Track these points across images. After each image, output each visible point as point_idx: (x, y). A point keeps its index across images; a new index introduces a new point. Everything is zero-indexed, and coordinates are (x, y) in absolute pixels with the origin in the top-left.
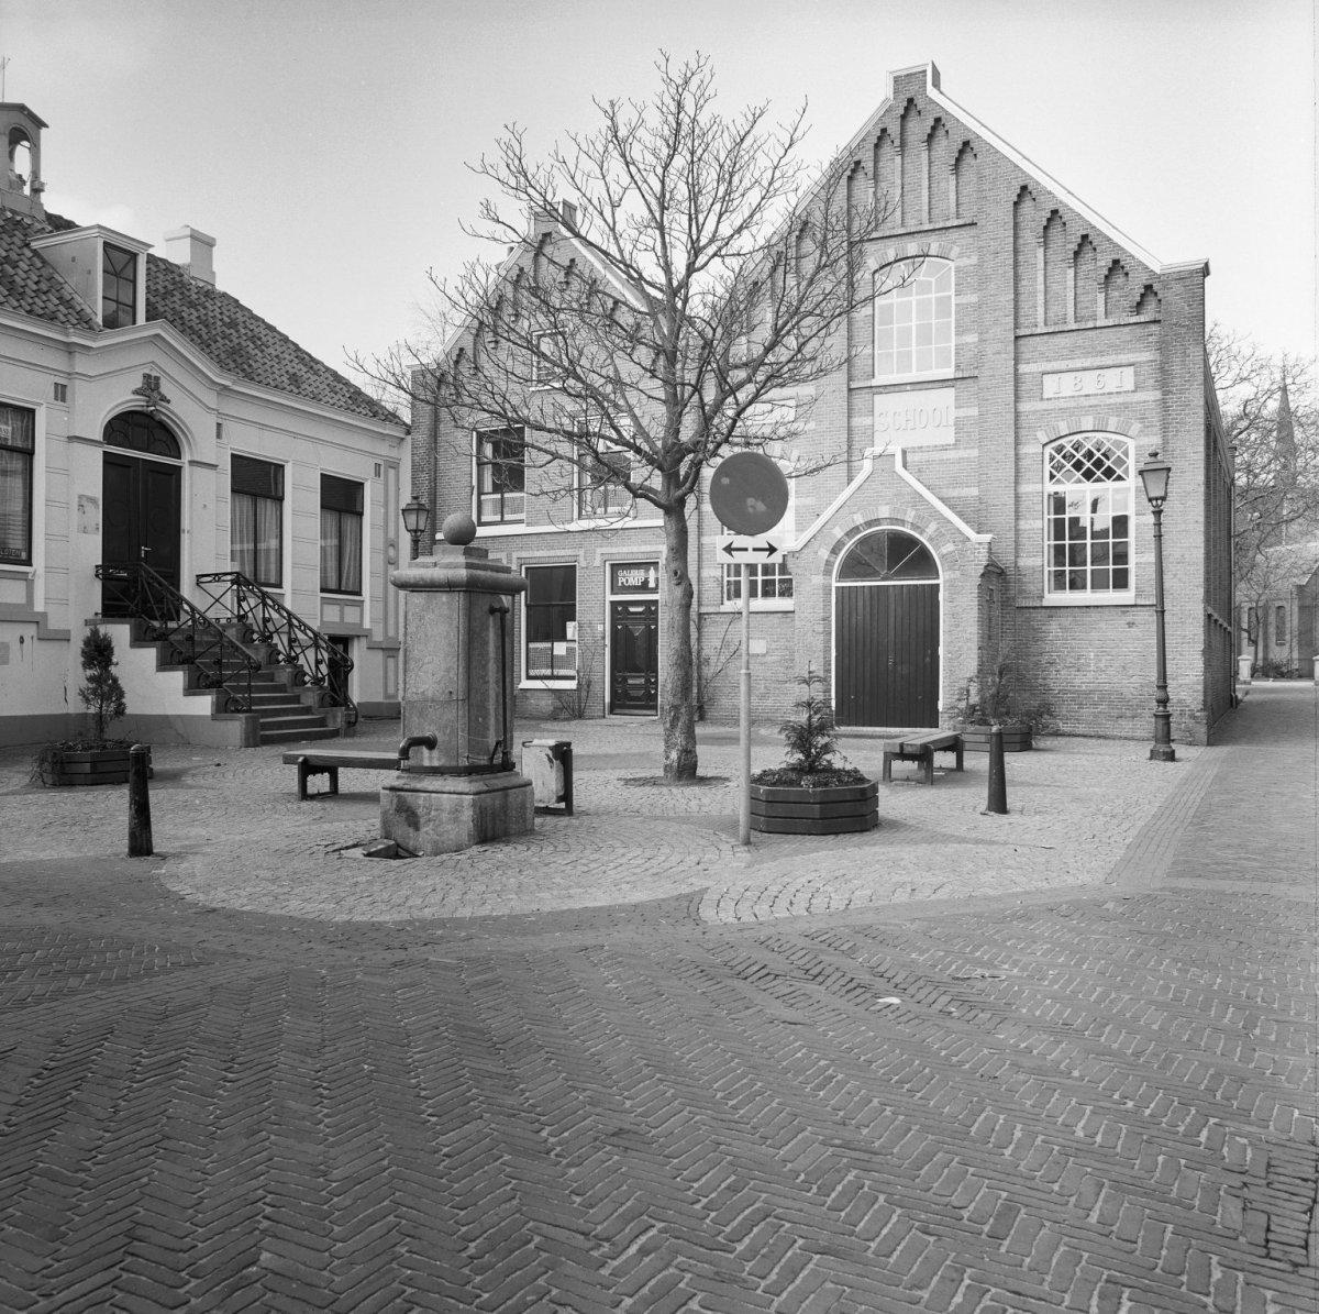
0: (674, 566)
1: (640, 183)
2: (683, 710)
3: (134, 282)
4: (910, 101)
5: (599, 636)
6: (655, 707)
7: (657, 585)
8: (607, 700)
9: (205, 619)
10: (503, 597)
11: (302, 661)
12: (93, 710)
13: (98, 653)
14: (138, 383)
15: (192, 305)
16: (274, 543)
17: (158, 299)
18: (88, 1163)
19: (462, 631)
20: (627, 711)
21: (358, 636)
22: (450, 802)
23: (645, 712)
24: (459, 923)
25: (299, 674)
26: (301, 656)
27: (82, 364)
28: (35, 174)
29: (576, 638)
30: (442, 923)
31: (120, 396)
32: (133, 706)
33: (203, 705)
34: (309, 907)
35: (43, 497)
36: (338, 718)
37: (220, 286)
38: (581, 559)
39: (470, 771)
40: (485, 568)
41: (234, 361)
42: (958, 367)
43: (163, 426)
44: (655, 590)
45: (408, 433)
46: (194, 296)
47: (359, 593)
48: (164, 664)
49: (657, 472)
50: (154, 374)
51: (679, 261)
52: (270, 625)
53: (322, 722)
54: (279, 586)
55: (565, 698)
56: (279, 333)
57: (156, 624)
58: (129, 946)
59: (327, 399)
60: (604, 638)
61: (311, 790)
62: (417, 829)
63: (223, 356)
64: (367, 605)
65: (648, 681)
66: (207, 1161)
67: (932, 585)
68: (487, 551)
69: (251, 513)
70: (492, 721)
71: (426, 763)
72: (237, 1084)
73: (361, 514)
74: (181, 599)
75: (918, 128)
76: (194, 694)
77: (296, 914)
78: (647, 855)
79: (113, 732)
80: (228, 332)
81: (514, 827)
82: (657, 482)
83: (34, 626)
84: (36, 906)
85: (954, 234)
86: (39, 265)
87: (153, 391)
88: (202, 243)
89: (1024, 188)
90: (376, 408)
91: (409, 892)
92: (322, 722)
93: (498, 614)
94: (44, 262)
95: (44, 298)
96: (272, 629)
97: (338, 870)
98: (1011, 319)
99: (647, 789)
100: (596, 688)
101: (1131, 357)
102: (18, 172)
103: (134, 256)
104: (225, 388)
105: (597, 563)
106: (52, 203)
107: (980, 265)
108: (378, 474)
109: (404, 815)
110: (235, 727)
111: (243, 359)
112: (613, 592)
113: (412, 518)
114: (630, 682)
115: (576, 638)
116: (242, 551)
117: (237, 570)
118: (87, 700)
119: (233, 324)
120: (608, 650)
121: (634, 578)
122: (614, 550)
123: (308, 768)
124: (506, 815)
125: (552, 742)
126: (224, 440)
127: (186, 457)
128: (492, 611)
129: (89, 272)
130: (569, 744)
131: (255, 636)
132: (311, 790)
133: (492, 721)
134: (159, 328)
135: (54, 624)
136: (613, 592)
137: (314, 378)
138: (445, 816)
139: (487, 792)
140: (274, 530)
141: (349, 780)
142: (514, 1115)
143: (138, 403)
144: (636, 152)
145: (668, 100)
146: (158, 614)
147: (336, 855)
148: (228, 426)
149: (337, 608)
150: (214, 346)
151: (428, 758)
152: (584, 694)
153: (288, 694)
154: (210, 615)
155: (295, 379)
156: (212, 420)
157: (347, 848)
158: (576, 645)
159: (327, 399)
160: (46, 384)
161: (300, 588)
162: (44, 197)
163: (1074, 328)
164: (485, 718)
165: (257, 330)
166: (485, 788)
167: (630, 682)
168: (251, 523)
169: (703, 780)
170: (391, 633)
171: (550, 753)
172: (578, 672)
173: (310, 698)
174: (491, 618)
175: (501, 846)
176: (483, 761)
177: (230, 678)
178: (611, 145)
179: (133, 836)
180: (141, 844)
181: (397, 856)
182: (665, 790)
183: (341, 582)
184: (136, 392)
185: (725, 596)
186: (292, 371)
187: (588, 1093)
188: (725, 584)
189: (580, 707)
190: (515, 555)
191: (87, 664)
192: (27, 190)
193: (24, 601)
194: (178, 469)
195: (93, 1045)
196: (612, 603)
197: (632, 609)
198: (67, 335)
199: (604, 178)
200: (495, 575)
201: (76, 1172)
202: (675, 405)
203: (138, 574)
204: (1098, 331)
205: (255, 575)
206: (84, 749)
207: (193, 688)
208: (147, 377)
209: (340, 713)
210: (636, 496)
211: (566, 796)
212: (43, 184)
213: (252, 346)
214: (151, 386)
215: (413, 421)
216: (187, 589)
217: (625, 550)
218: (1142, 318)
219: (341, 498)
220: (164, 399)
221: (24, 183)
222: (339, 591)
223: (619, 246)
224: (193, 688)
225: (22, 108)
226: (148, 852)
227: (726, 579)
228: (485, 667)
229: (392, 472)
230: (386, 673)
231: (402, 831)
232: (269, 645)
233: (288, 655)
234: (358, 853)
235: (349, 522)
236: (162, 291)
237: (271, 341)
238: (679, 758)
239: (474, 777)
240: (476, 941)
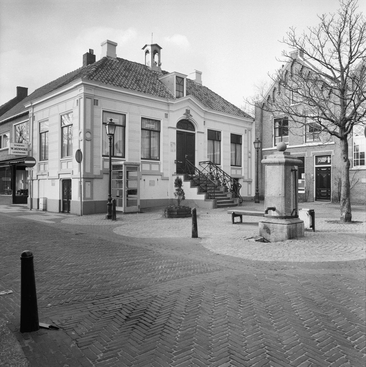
0: (344, 156)
1: (332, 39)
2: (347, 200)
3: (183, 86)
5: (312, 178)
6: (330, 199)
7: (330, 162)
8: (314, 196)
9: (202, 173)
10: (295, 166)
11: (227, 185)
12: (177, 198)
13: (178, 183)
14: (185, 112)
15: (197, 90)
16: (218, 153)
17: (188, 89)
18: (210, 327)
19: (283, 177)
20: (320, 200)
21: (241, 178)
22: (281, 228)
23: (326, 200)
24: (291, 264)
25: (226, 188)
26: (227, 184)
27: (171, 108)
28: (159, 61)
29: (305, 178)
30: (285, 263)
31: (180, 116)
32: (187, 197)
33: (202, 197)
34: (244, 255)
35: (128, 149)
36: (237, 201)
37: (203, 85)
38: (306, 155)
39: (286, 218)
40: (290, 158)
41: (208, 104)
44: (330, 163)
45: (254, 121)
46: (197, 88)
47: (241, 166)
48: (193, 186)
49: (338, 127)
50: (188, 109)
51: (345, 61)
52: (218, 175)
53: (233, 202)
54: (220, 164)
55: (301, 196)
56: (219, 96)
57: (190, 175)
58: (199, 263)
59: (231, 113)
60: (313, 178)
61: (235, 221)
62: (270, 234)
63: (205, 103)
64: (243, 170)
65: (327, 191)
66: (243, 331)
68: (290, 153)
69: (212, 145)
70: (292, 203)
71: (272, 215)
72: (244, 308)
73: (241, 144)
74: (195, 168)
76: (200, 194)
77: (241, 257)
78: (344, 245)
79: (182, 204)
80: (206, 97)
81: (298, 235)
82: (338, 130)
83: (160, 176)
84: (172, 250)
86: (161, 84)
88: (199, 74)
90: (245, 114)
91: (272, 253)
92: (233, 202)
93: (294, 171)
94: (162, 83)
95: (162, 92)
96: (219, 176)
97: (249, 245)
99: (336, 224)
100: (311, 193)
102: (155, 61)
103: (183, 79)
104: (206, 111)
105: (311, 155)
106: (163, 68)
108: (246, 133)
109: (266, 230)
110: (211, 203)
111: (210, 104)
113: (256, 145)
114: (322, 191)
115: (305, 178)
116: (210, 155)
117: (209, 160)
118: (176, 195)
119: (207, 94)
120: (315, 182)
121: (323, 160)
122: (317, 152)
123: (234, 215)
124: (296, 231)
125: (308, 210)
126: (206, 126)
127: (196, 131)
128: (292, 170)
129: (172, 84)
130: (313, 210)
131: (214, 178)
132: (235, 221)
133: (292, 203)
134: (190, 97)
135: (165, 176)
136: (316, 164)
137: (228, 107)
138: (278, 231)
139: (291, 224)
140: (218, 150)
141: (245, 219)
142: (335, 331)
144: (331, 29)
145: (341, 11)
146: (190, 173)
147: (247, 240)
148: (207, 122)
149: (235, 170)
150: (203, 101)
151: (273, 213)
152: (307, 195)
153: (225, 194)
154: (203, 172)
155: (223, 108)
156: (203, 120)
157: (250, 238)
158: (305, 180)
159: (231, 113)
160: (163, 114)
161: (225, 164)
162: (161, 67)
164: (290, 202)
165: (213, 96)
166: (290, 223)
167: (322, 191)
168: (213, 149)
169: (353, 222)
170: (250, 177)
171: (308, 213)
172: (305, 188)
173: (229, 195)
174: (292, 173)
175: (296, 240)
176: (289, 215)
177: (210, 190)
178: (322, 28)
179: (193, 232)
180: (195, 235)
181: (264, 242)
182: (342, 225)
183: (236, 164)
184: (184, 114)
185: (353, 165)
186: (222, 106)
187: (358, 326)
188: (353, 161)
189: (306, 198)
191: (176, 186)
192: (157, 65)
193: (158, 170)
194: (194, 134)
195: (200, 292)
196: (316, 167)
197: (322, 169)
198: (168, 101)
199: (319, 39)
200: (293, 160)
201: (208, 329)
202: (344, 106)
203: (185, 163)
205: (214, 162)
206: (175, 208)
207: (200, 192)
208: (187, 110)
209: (238, 199)
210: (332, 134)
211: (313, 226)
212: (161, 63)
213: (212, 100)
214: (188, 112)
215: (255, 117)
216: (197, 165)
217: (320, 152)
219: (236, 140)
220: (191, 116)
221: (157, 63)
222: (235, 166)
223: (324, 59)
224: (200, 192)
225: (156, 45)
226: (197, 237)
227: (354, 159)
228: (290, 187)
229: (249, 132)
230: (248, 188)
231: (265, 235)
232: (218, 181)
233: (223, 184)
234: (253, 240)
235: (238, 146)
236: (189, 87)
237: (217, 98)
238: (346, 215)
239: (287, 219)
240: (297, 269)
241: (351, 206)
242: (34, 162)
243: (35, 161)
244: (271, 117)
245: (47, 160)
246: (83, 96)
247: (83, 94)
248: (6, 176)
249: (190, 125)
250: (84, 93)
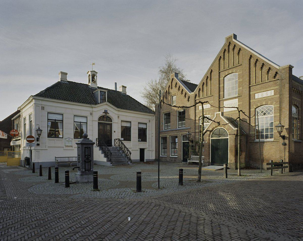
4: (230, 42)
31: (101, 113)
40: (89, 141)
42: (239, 94)
48: (102, 153)
67: (227, 138)
75: (231, 47)
85: (238, 67)
89: (251, 56)
98: (248, 83)
101: (273, 88)
107: (243, 73)
112: (183, 141)
127: (113, 122)
143: (104, 114)
156: (117, 116)
163: (261, 83)
190: (169, 134)
204: (266, 83)
214: (106, 112)
218: (275, 79)
225: (94, 71)
227: (256, 134)
248: (3, 147)
249: (108, 119)
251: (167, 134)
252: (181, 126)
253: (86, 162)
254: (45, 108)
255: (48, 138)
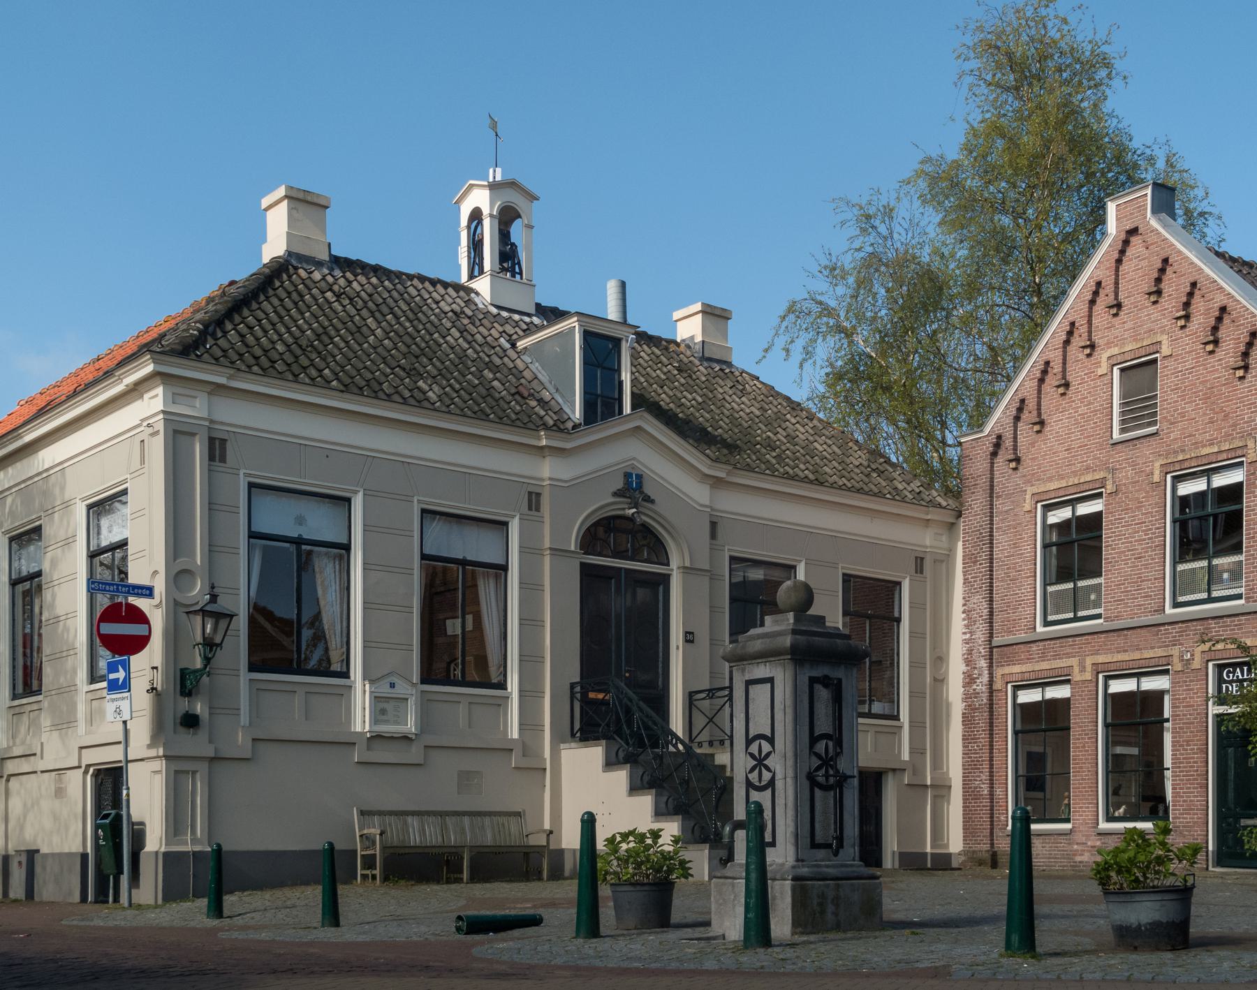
21: (894, 770)
38: (1176, 660)
43: (646, 529)
87: (635, 490)
136: (1221, 701)
169: (1208, 943)
190: (1089, 661)
196: (1218, 716)
220: (648, 499)
241: (1033, 827)
242: (108, 628)
243: (264, 525)
244: (1028, 496)
245: (39, 692)
246: (160, 426)
247: (161, 416)
250: (163, 412)
251: (1074, 661)
252: (1071, 615)
253: (821, 787)
254: (228, 445)
255: (250, 670)
